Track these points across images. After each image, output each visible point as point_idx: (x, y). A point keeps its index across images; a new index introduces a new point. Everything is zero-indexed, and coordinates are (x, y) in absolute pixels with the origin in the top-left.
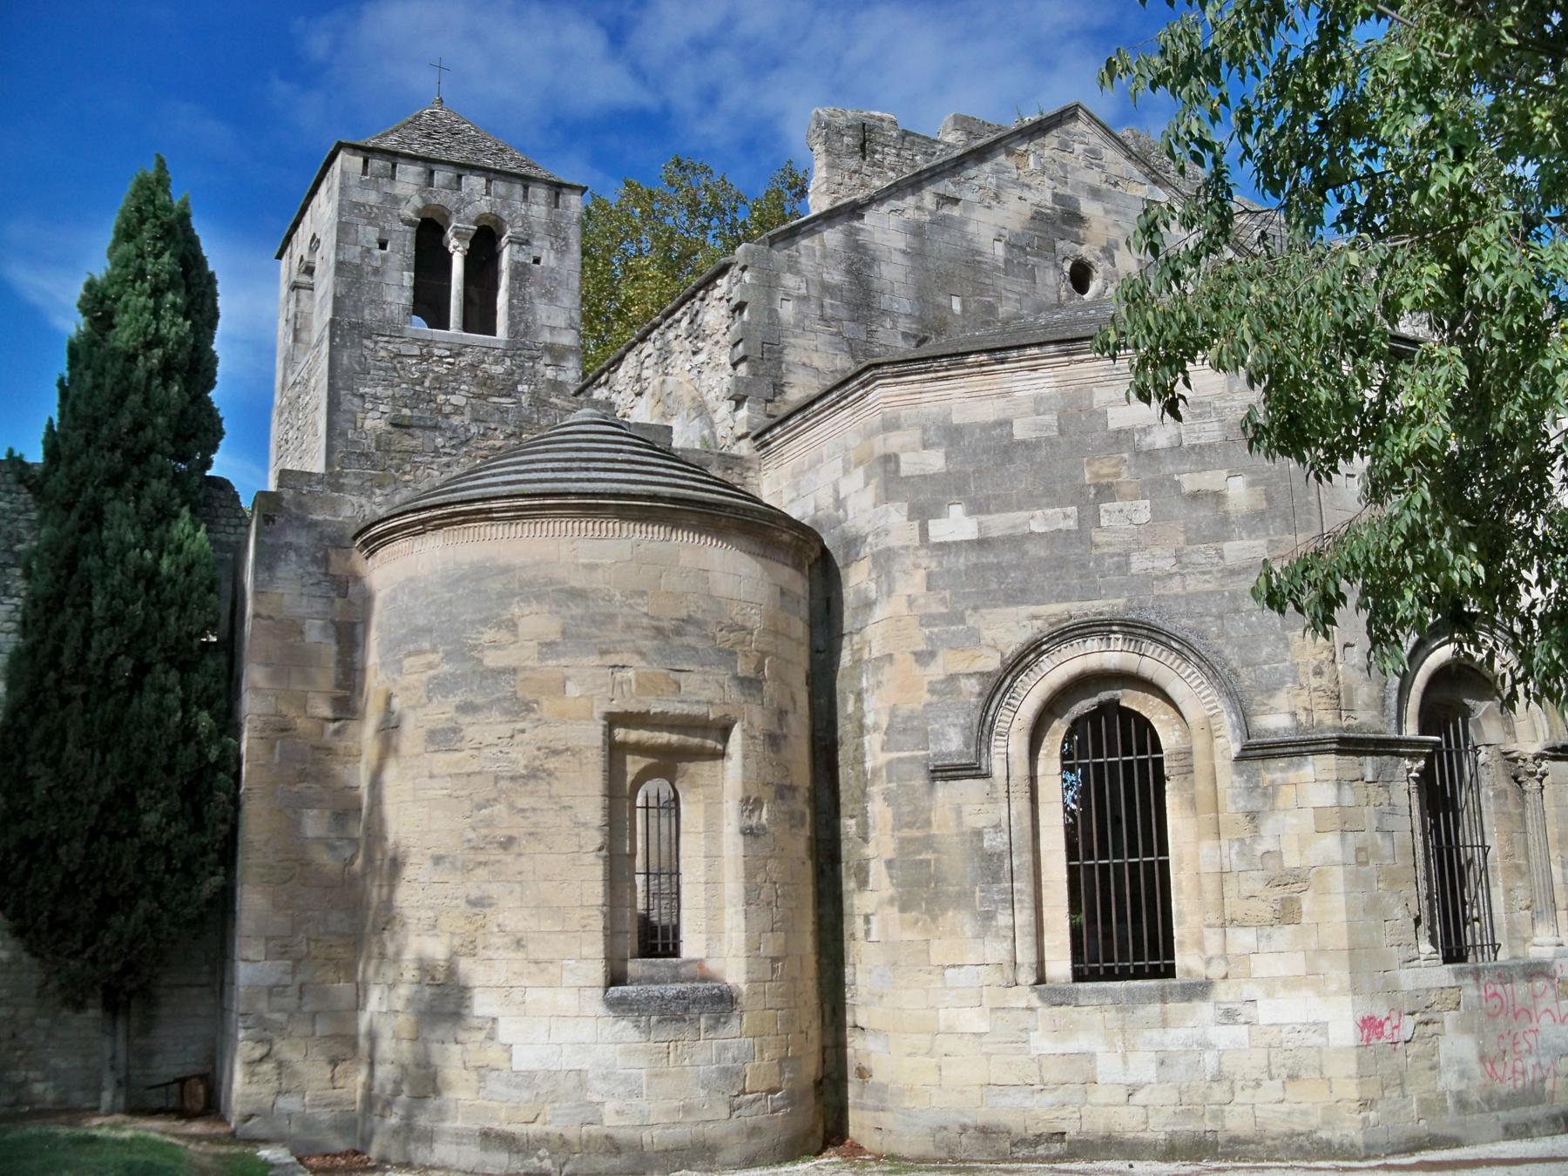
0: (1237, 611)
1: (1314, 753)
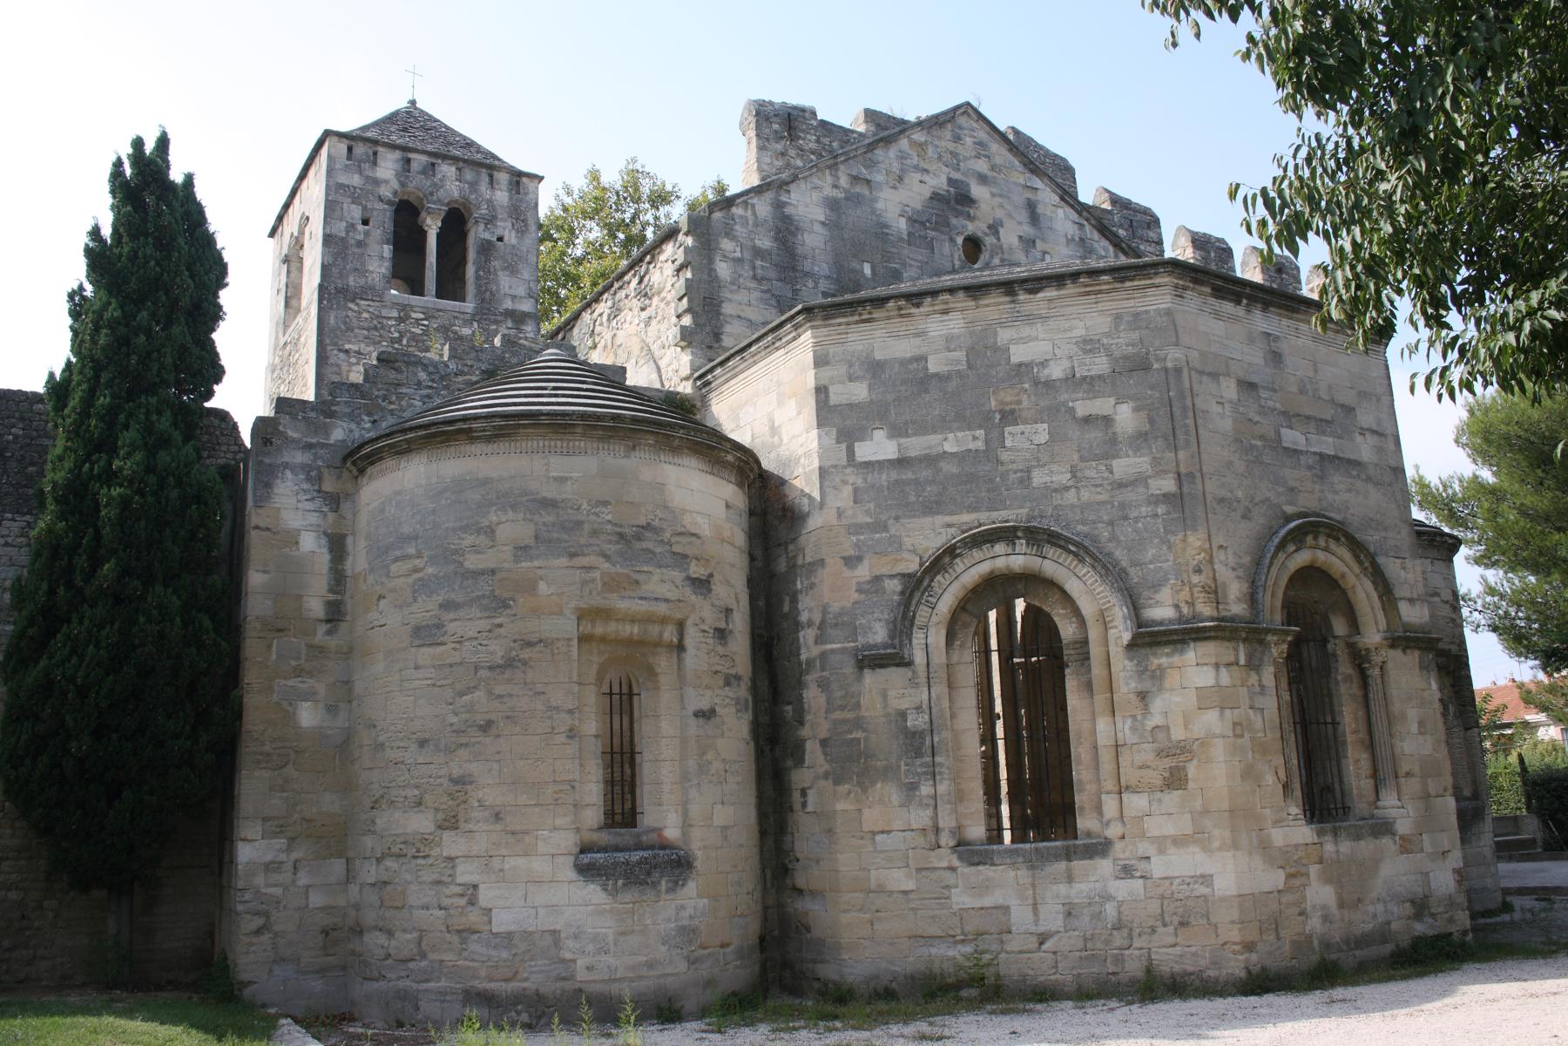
0: (1126, 518)
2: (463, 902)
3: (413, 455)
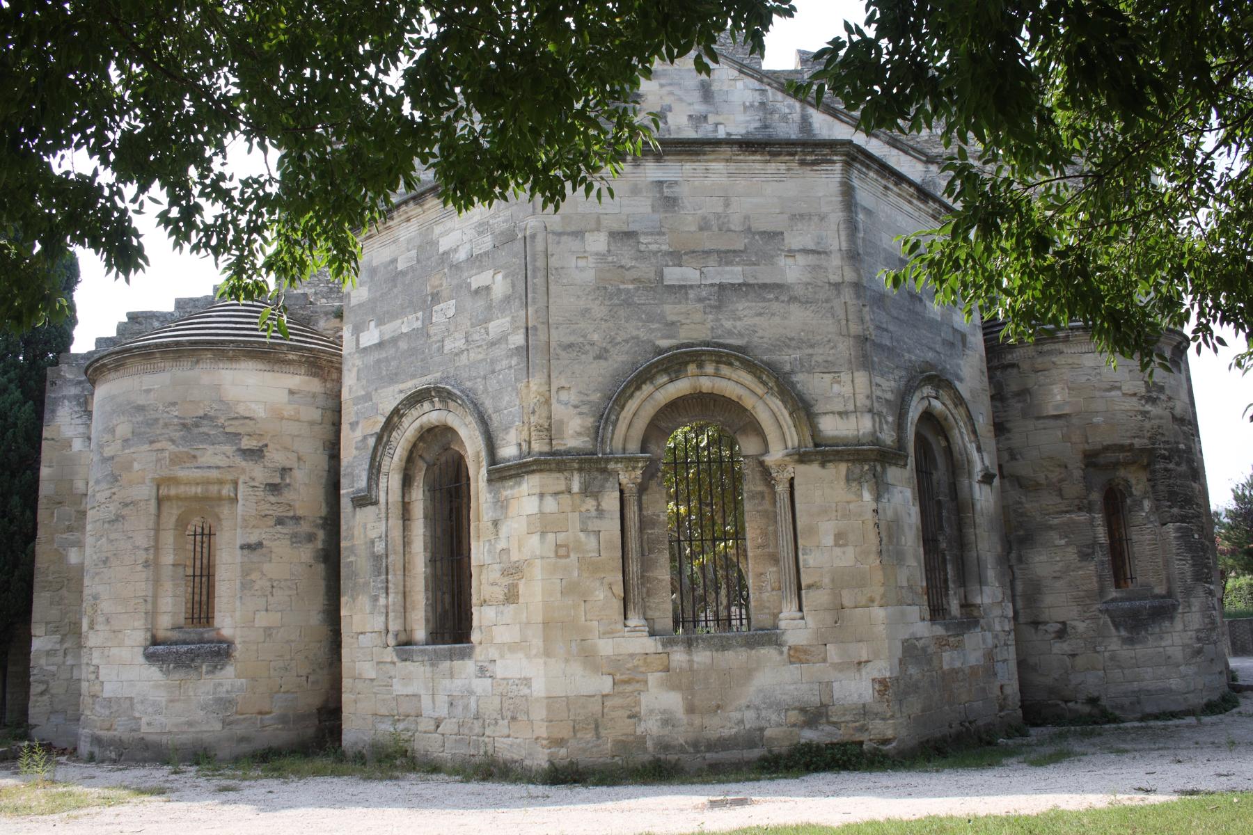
0: (493, 372)
1: (528, 473)
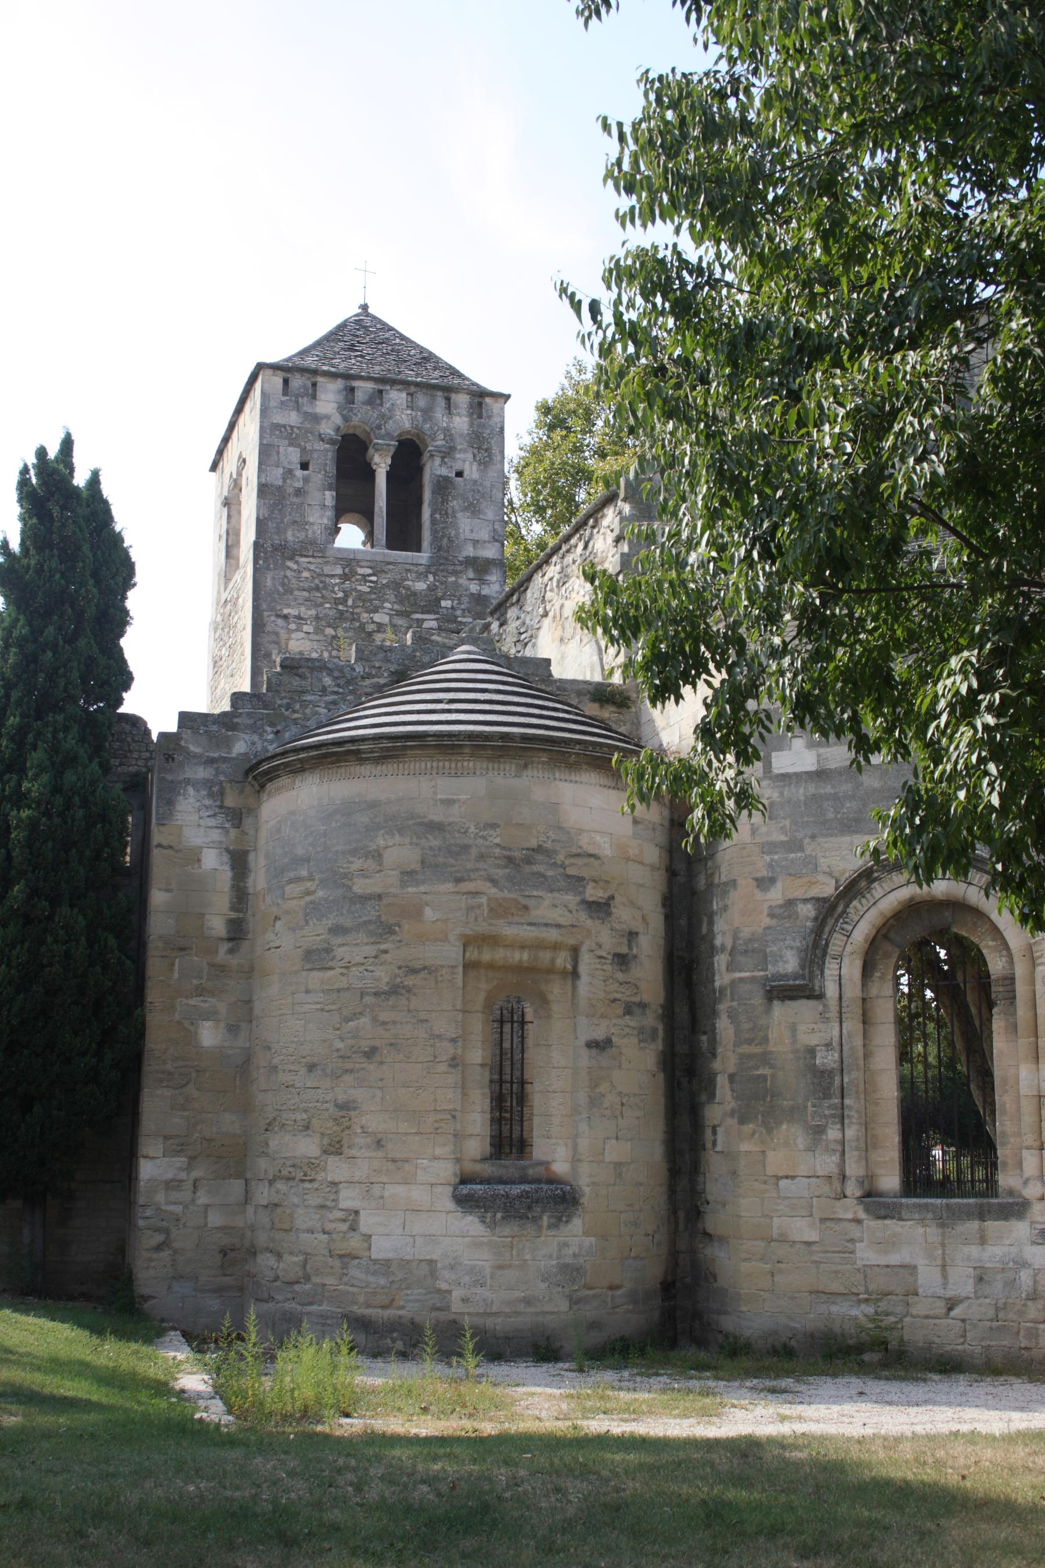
2: (344, 1227)
3: (307, 774)
